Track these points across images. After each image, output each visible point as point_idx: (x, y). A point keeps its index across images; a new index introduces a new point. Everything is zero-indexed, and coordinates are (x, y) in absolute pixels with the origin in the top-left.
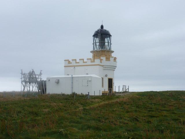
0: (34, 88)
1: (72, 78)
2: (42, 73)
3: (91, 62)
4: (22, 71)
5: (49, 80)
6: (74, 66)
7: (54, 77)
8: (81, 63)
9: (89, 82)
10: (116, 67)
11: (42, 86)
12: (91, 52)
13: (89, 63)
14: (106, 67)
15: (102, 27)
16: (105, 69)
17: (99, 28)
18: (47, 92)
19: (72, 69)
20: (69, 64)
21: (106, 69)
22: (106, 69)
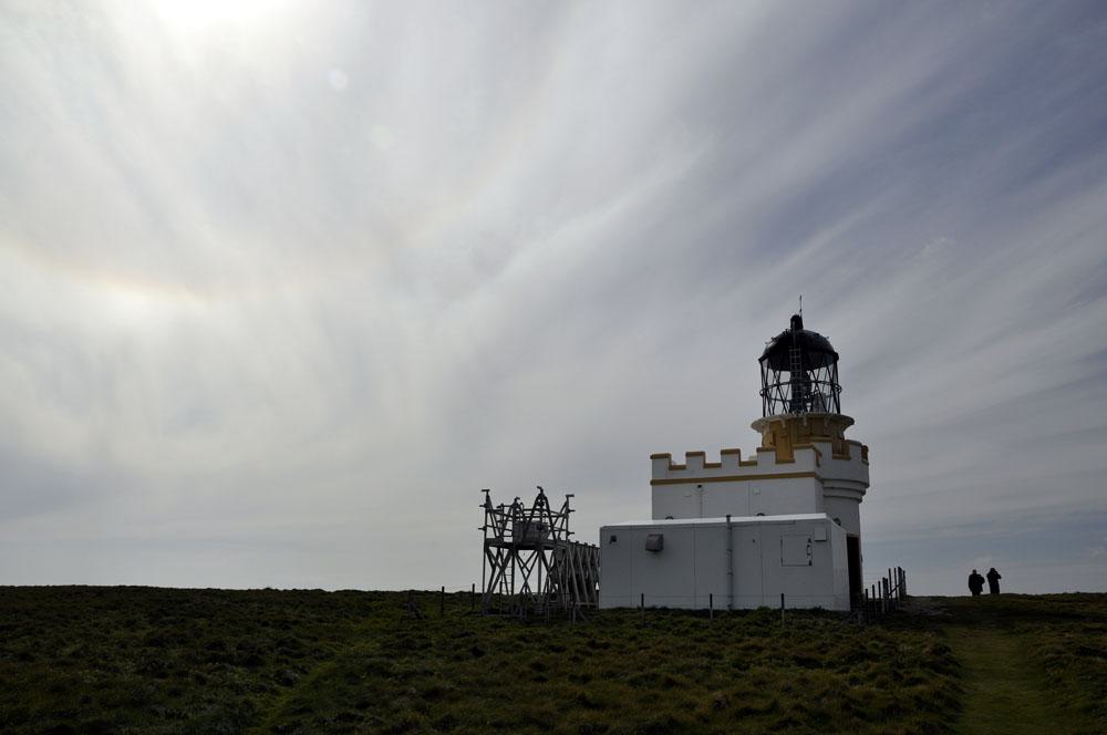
0: (530, 577)
1: (731, 526)
2: (570, 508)
3: (778, 462)
4: (488, 497)
5: (614, 539)
6: (699, 481)
8: (732, 470)
12: (756, 426)
13: (769, 465)
14: (832, 488)
15: (797, 321)
20: (668, 475)
21: (837, 493)
22: (837, 493)
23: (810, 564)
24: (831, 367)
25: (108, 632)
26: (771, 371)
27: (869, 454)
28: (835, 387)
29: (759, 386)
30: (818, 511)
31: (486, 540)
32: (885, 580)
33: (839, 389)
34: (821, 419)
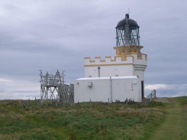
0: (54, 94)
1: (111, 80)
3: (122, 60)
4: (41, 72)
5: (90, 87)
7: (175, 97)
9: (40, 71)
10: (146, 66)
11: (68, 93)
12: (114, 48)
14: (137, 67)
15: (127, 16)
16: (136, 69)
17: (123, 17)
18: (76, 101)
19: (95, 69)
22: (138, 69)
23: (132, 90)
24: (137, 30)
25: (146, 112)
26: (119, 30)
27: (147, 57)
28: (138, 37)
29: (116, 36)
30: (134, 75)
31: (41, 85)
32: (151, 94)
33: (139, 37)
34: (134, 47)
